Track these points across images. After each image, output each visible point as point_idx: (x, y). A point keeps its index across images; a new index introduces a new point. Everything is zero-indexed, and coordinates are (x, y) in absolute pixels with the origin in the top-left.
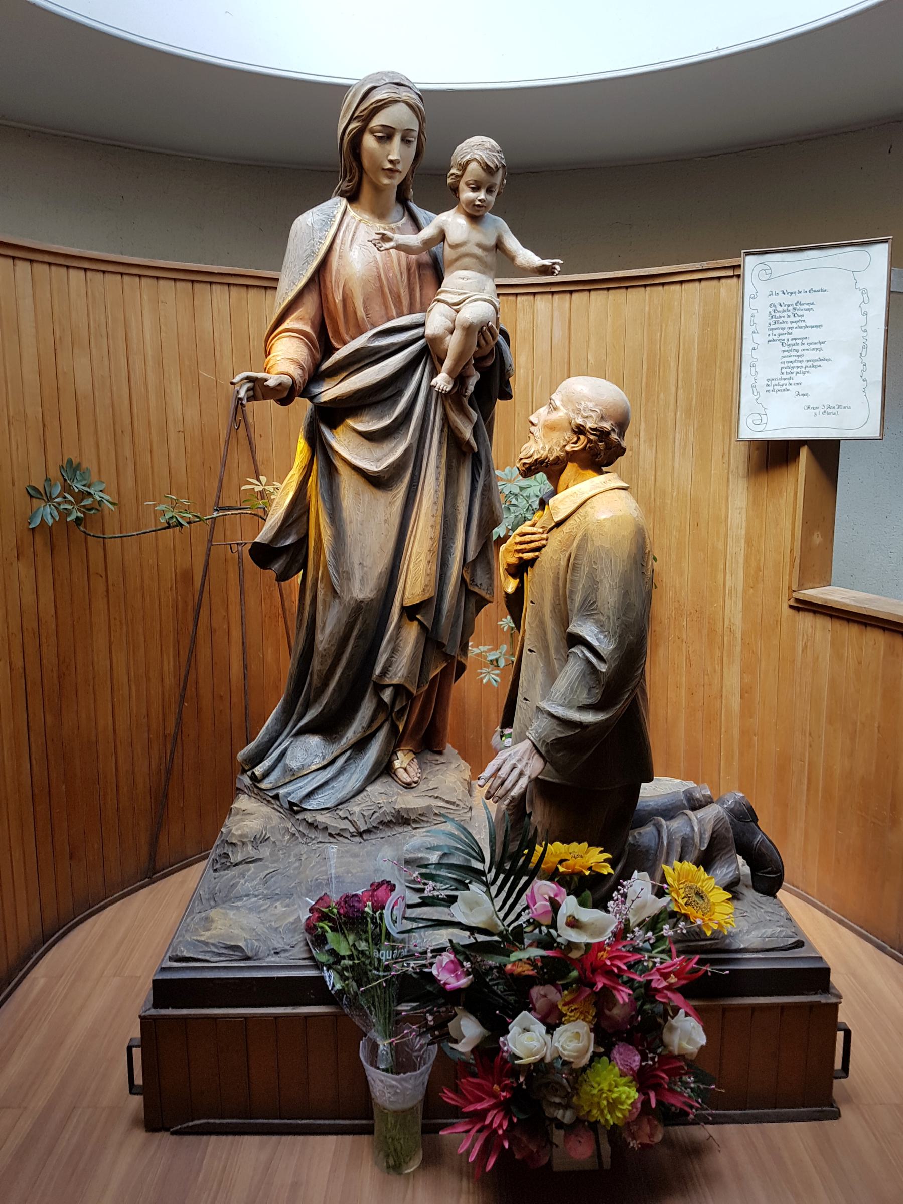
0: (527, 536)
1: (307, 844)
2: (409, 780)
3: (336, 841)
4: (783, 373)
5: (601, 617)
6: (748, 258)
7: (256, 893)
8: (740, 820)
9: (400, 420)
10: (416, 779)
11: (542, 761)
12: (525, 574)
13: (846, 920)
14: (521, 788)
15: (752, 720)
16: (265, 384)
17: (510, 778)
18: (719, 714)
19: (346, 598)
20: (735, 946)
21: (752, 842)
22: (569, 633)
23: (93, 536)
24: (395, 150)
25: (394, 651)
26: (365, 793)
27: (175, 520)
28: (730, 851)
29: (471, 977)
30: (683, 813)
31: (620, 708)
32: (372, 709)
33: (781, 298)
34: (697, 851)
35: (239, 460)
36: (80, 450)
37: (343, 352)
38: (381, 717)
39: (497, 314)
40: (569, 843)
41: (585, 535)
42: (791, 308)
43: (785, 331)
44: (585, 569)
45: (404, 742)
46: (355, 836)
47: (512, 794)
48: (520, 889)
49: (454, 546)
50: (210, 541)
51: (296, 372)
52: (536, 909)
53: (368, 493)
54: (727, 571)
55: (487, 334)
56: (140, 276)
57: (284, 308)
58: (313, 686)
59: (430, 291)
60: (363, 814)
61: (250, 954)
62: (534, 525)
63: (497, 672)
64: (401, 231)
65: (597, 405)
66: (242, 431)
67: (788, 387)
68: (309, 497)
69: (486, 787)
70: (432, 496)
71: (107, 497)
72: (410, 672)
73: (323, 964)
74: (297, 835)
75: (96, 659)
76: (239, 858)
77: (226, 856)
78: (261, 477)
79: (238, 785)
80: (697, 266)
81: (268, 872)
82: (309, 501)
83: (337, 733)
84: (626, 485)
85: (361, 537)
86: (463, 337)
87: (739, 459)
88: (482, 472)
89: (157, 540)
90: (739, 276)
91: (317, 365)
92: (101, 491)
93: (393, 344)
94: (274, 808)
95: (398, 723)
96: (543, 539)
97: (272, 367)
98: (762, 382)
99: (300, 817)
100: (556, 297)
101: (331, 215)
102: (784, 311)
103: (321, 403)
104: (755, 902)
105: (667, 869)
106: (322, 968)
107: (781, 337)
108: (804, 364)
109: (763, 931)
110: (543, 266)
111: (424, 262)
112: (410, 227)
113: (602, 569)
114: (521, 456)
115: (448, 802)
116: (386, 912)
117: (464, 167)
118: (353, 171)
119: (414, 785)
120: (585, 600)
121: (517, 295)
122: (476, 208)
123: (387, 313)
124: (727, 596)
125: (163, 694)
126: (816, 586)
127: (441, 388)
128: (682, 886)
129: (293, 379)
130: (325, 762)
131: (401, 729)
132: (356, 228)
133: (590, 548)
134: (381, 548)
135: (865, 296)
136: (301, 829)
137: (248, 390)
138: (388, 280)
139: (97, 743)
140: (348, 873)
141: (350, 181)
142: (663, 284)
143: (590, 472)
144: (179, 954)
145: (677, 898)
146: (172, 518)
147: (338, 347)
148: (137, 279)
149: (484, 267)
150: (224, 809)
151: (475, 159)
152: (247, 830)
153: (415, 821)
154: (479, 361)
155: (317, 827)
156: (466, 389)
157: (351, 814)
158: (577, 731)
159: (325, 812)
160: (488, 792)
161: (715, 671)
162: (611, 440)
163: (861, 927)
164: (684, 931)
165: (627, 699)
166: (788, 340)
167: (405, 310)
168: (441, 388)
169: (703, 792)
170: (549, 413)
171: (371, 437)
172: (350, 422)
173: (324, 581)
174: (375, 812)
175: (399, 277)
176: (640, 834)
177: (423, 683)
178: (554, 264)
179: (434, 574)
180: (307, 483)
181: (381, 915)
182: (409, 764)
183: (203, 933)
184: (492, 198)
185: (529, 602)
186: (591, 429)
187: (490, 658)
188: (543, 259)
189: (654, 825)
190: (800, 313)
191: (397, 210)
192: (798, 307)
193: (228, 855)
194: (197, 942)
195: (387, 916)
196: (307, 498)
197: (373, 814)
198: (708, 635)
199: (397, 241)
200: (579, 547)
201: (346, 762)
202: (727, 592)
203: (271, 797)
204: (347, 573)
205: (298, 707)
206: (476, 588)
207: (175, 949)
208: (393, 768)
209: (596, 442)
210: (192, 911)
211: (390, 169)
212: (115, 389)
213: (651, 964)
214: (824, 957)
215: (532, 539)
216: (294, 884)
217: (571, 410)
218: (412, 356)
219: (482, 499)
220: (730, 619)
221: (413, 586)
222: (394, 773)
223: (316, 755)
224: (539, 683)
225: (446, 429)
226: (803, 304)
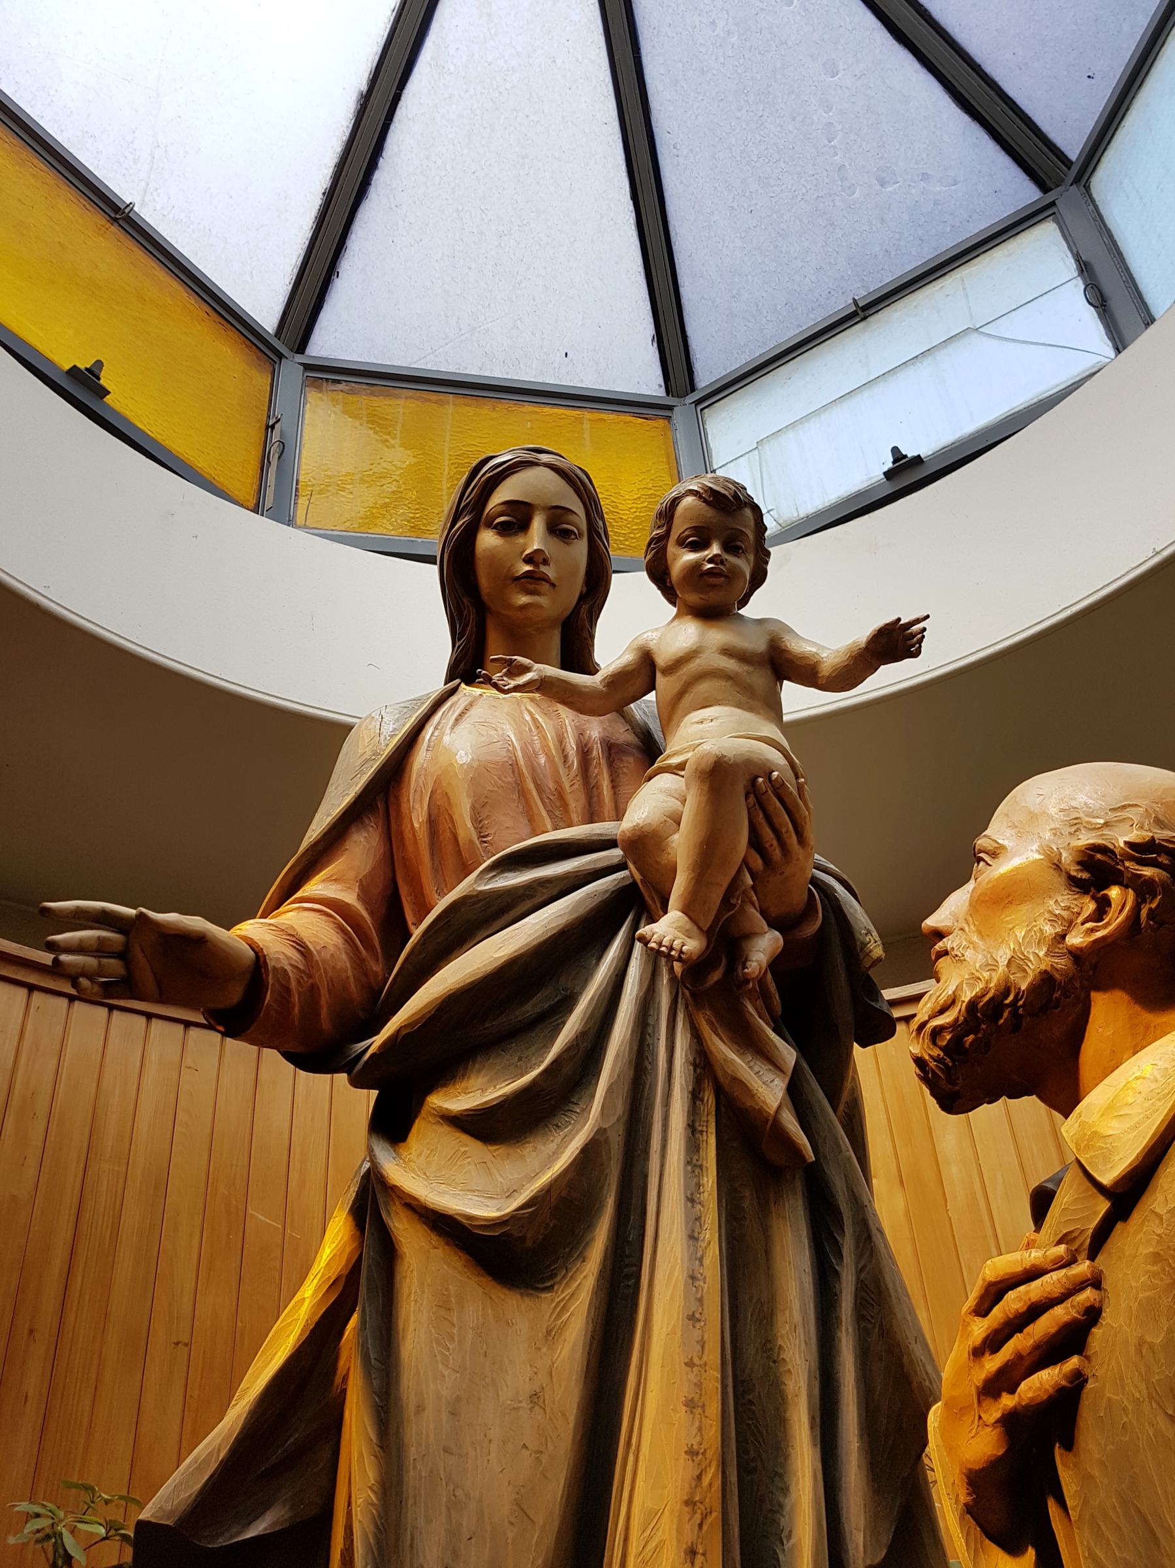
0: (1011, 1295)
9: (567, 1070)
12: (1053, 1508)
70: (680, 1292)
82: (344, 1391)
86: (704, 799)
88: (848, 1244)
134: (517, 1503)
196: (338, 1379)
225: (709, 1097)
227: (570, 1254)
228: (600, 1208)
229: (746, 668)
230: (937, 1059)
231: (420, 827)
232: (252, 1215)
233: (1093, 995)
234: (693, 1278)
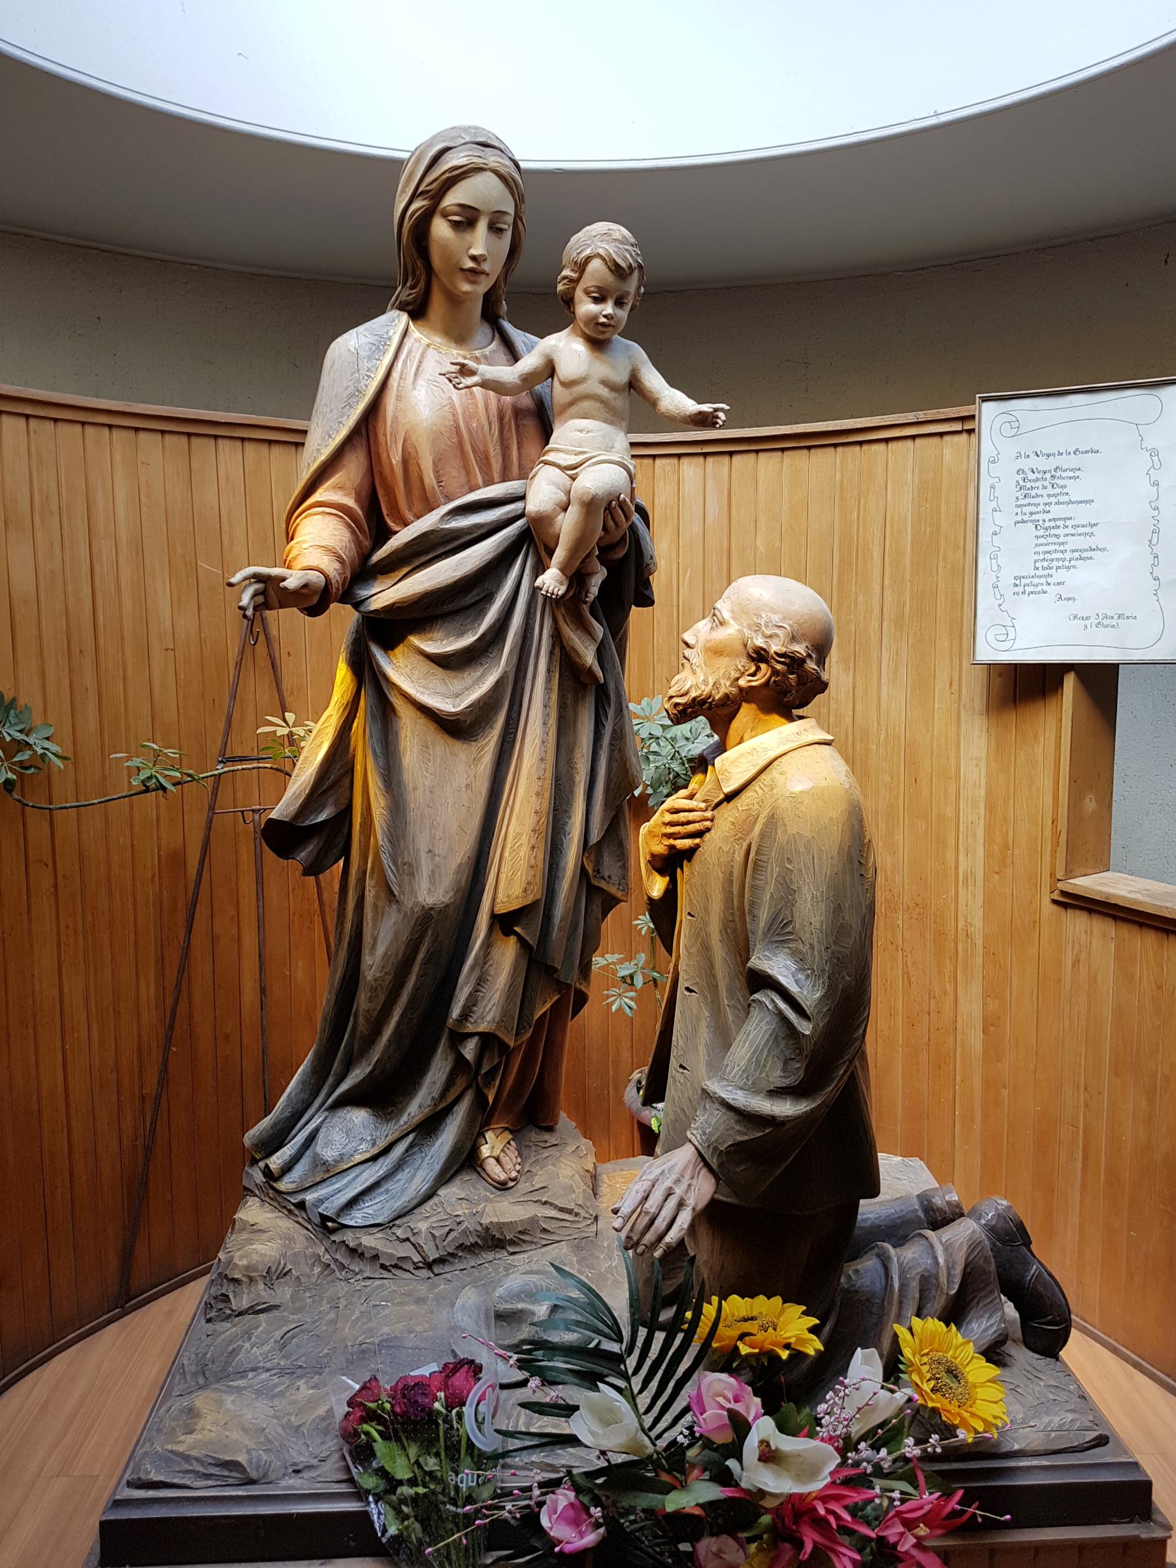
0: (682, 814)
1: (347, 1280)
2: (503, 1177)
3: (392, 1276)
4: (1038, 569)
5: (801, 947)
6: (985, 405)
7: (268, 1365)
8: (1004, 1243)
9: (488, 637)
10: (514, 1174)
11: (713, 1180)
12: (679, 870)
13: (1144, 1363)
14: (682, 1229)
15: (1000, 1064)
16: (282, 584)
17: (664, 1213)
18: (952, 1054)
19: (408, 903)
20: (1006, 1448)
21: (1024, 1277)
22: (750, 969)
23: (33, 806)
24: (479, 241)
25: (481, 981)
26: (435, 1200)
27: (154, 781)
28: (992, 1291)
29: (602, 1530)
30: (920, 1234)
31: (831, 1092)
32: (448, 1069)
33: (1034, 462)
34: (944, 1297)
35: (257, 688)
36: (16, 678)
37: (403, 537)
38: (461, 1083)
39: (632, 482)
40: (752, 1297)
41: (772, 817)
42: (1048, 475)
43: (1040, 508)
44: (773, 870)
45: (495, 1119)
46: (422, 1268)
47: (667, 1239)
48: (674, 1354)
49: (570, 822)
50: (212, 808)
51: (331, 567)
52: (704, 1419)
53: (442, 745)
54: (961, 848)
55: (617, 512)
56: (110, 426)
57: (315, 471)
58: (358, 1035)
59: (531, 448)
60: (433, 1235)
61: (254, 1475)
62: (691, 797)
63: (632, 994)
64: (488, 360)
65: (784, 618)
66: (261, 648)
67: (1045, 588)
68: (354, 749)
69: (623, 1235)
71: (54, 748)
72: (505, 1013)
73: (368, 1492)
74: (333, 1266)
75: (37, 988)
76: (245, 1303)
77: (225, 1298)
78: (286, 714)
79: (246, 1183)
80: (910, 417)
81: (286, 1329)
82: (354, 755)
83: (394, 1104)
84: (830, 737)
85: (430, 810)
87: (974, 690)
88: (611, 713)
89: (131, 808)
91: (365, 556)
92: (47, 739)
94: (298, 1222)
95: (485, 1091)
96: (707, 820)
97: (295, 558)
98: (1007, 580)
99: (336, 1238)
100: (710, 460)
101: (386, 336)
102: (1037, 480)
103: (376, 611)
104: (1029, 1368)
105: (901, 1331)
106: (367, 1498)
107: (1035, 517)
108: (1068, 555)
109: (1046, 1419)
110: (700, 413)
111: (523, 407)
112: (502, 355)
114: (671, 692)
115: (562, 1210)
116: (468, 1410)
117: (581, 267)
118: (418, 272)
119: (511, 1184)
121: (654, 457)
122: (601, 328)
123: (469, 481)
124: (961, 883)
125: (139, 1036)
126: (1089, 871)
127: (550, 591)
128: (925, 1359)
129: (327, 577)
130: (375, 1151)
131: (491, 1101)
132: (423, 356)
133: (781, 837)
136: (338, 1257)
137: (255, 595)
138: (470, 433)
139: (40, 1112)
140: (410, 1332)
141: (412, 288)
142: (861, 443)
143: (776, 718)
144: (143, 1477)
145: (919, 1383)
146: (150, 778)
147: (397, 529)
148: (106, 431)
149: (612, 415)
150: (225, 1223)
152: (255, 1258)
153: (512, 1243)
154: (605, 551)
155: (363, 1254)
156: (587, 592)
157: (414, 1234)
158: (767, 1131)
159: (375, 1230)
160: (629, 1238)
161: (946, 993)
162: (806, 671)
163: (1169, 1376)
164: (939, 1450)
165: (843, 1075)
166: (1044, 521)
167: (496, 475)
168: (550, 591)
169: (947, 1198)
170: (712, 629)
171: (445, 662)
172: (414, 640)
173: (375, 875)
174: (451, 1230)
175: (486, 428)
176: (857, 1271)
177: (524, 1028)
178: (716, 410)
179: (541, 865)
180: (350, 729)
181: (460, 1416)
182: (502, 1150)
183: (182, 1438)
184: (623, 314)
185: (685, 914)
186: (776, 653)
187: (621, 974)
188: (699, 403)
189: (878, 1256)
190: (1061, 482)
191: (483, 332)
192: (1058, 475)
193: (228, 1296)
194: (172, 1456)
195: (469, 1417)
196: (351, 750)
197: (448, 1233)
198: (934, 941)
199: (482, 375)
200: (762, 835)
201: (407, 1151)
202: (961, 877)
203: (294, 1204)
204: (410, 865)
205: (336, 1064)
206: (603, 881)
207: (137, 1468)
208: (479, 1158)
209: (784, 675)
210: (168, 1395)
211: (472, 270)
212: (70, 589)
213: (886, 1503)
214: (1141, 1462)
215: (690, 819)
216: (326, 1351)
217: (745, 625)
218: (506, 543)
219: (611, 751)
220: (966, 918)
221: (510, 882)
222: (481, 1166)
223: (362, 1140)
224: (703, 1042)
225: (557, 651)
226: (1065, 470)
228: (502, 706)
229: (614, 395)
230: (675, 715)
232: (201, 566)
234: (544, 742)
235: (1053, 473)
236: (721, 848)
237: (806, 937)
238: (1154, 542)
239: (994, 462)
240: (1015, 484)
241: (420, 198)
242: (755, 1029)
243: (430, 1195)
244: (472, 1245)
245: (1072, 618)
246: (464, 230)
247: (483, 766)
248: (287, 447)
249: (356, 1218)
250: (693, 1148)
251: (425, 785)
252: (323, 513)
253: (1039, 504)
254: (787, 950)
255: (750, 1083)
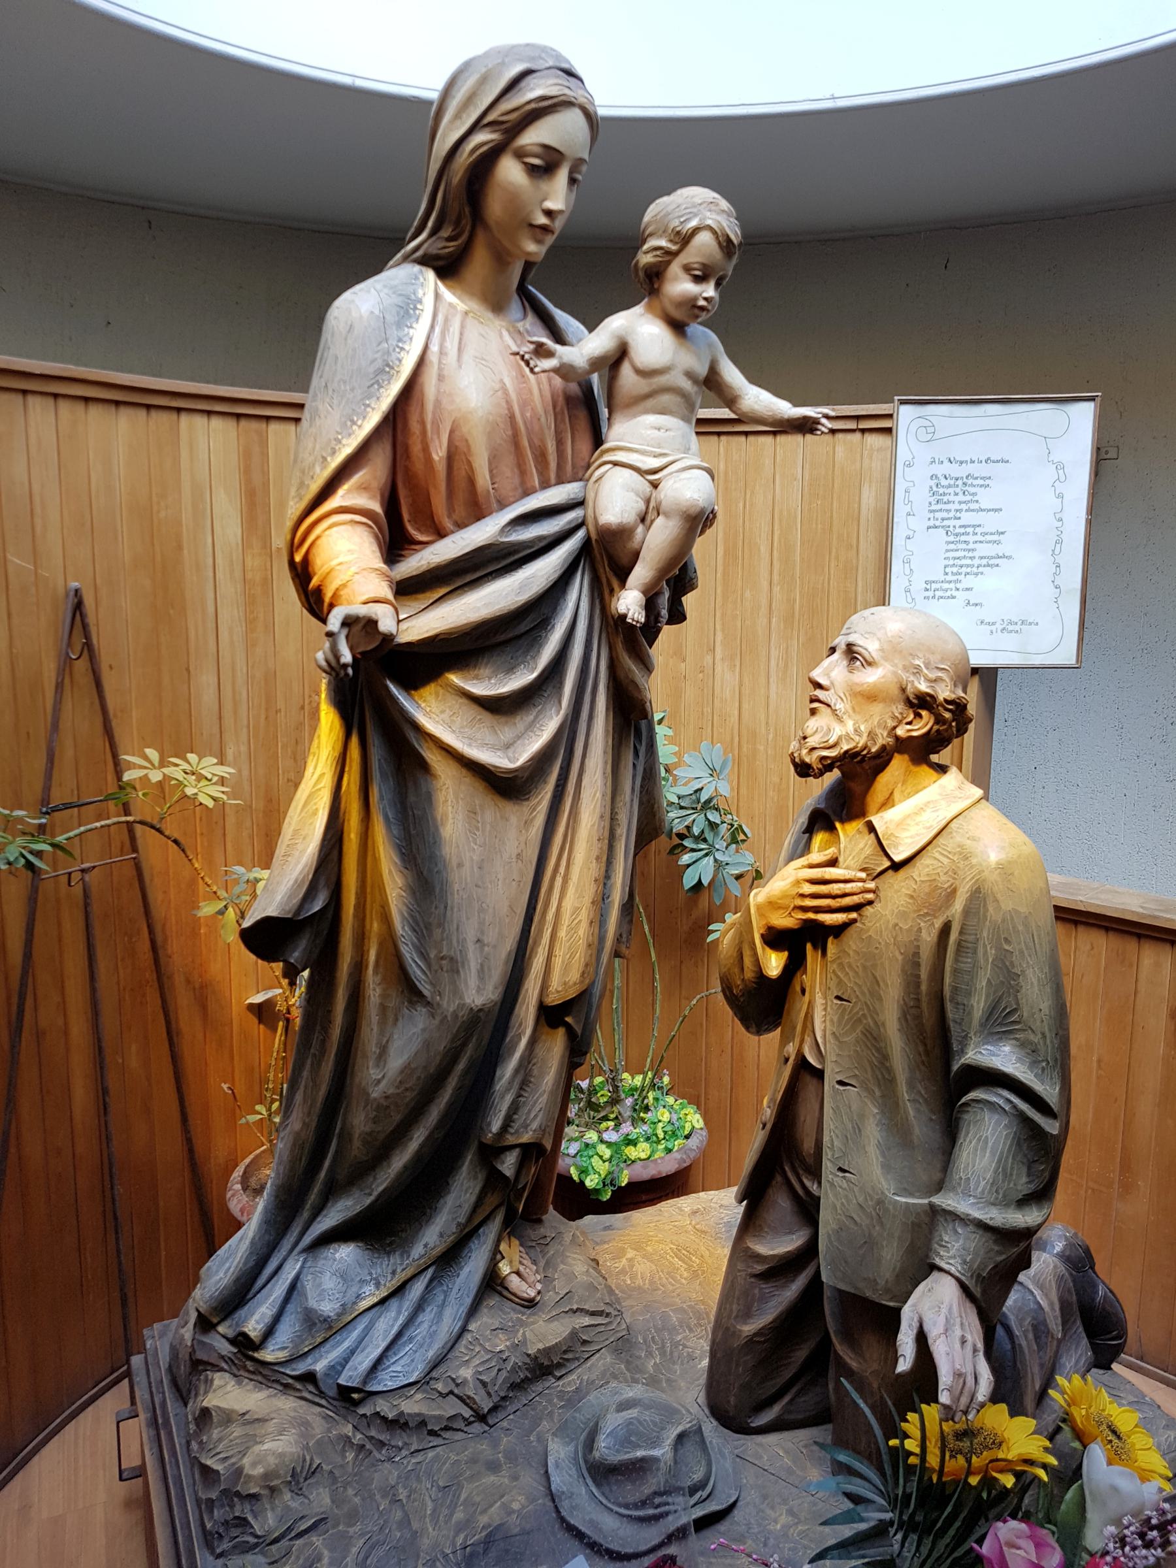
1: (390, 1459)
4: (947, 574)
5: (1032, 1037)
10: (539, 1286)
21: (1093, 1300)
26: (468, 1337)
33: (947, 468)
41: (978, 890)
42: (960, 482)
43: (951, 515)
44: (987, 954)
46: (473, 1422)
53: (492, 809)
60: (481, 1381)
67: (954, 593)
74: (368, 1446)
85: (480, 890)
90: (888, 431)
93: (540, 538)
98: (918, 585)
102: (949, 486)
107: (946, 523)
108: (976, 562)
113: (1021, 952)
115: (593, 1314)
118: (464, 222)
120: (994, 1008)
123: (523, 482)
135: (1061, 472)
136: (373, 1433)
138: (525, 423)
151: (710, 228)
152: (272, 1461)
153: (559, 1366)
155: (406, 1424)
157: (457, 1385)
167: (553, 480)
172: (454, 678)
186: (946, 701)
190: (972, 490)
193: (245, 1519)
200: (966, 912)
217: (901, 666)
224: (873, 1142)
226: (976, 478)
227: (539, 781)
231: (440, 461)
233: (896, 755)
235: (965, 480)
236: (897, 925)
237: (1037, 1025)
238: (1057, 552)
239: (909, 466)
240: (928, 488)
241: (488, 129)
242: (993, 1135)
243: (464, 1330)
244: (523, 1381)
245: (979, 623)
246: (540, 177)
247: (535, 829)
248: (106, 406)
249: (386, 1381)
250: (953, 1281)
251: (472, 860)
252: (353, 522)
253: (950, 511)
254: (1014, 1042)
255: (1000, 1196)
